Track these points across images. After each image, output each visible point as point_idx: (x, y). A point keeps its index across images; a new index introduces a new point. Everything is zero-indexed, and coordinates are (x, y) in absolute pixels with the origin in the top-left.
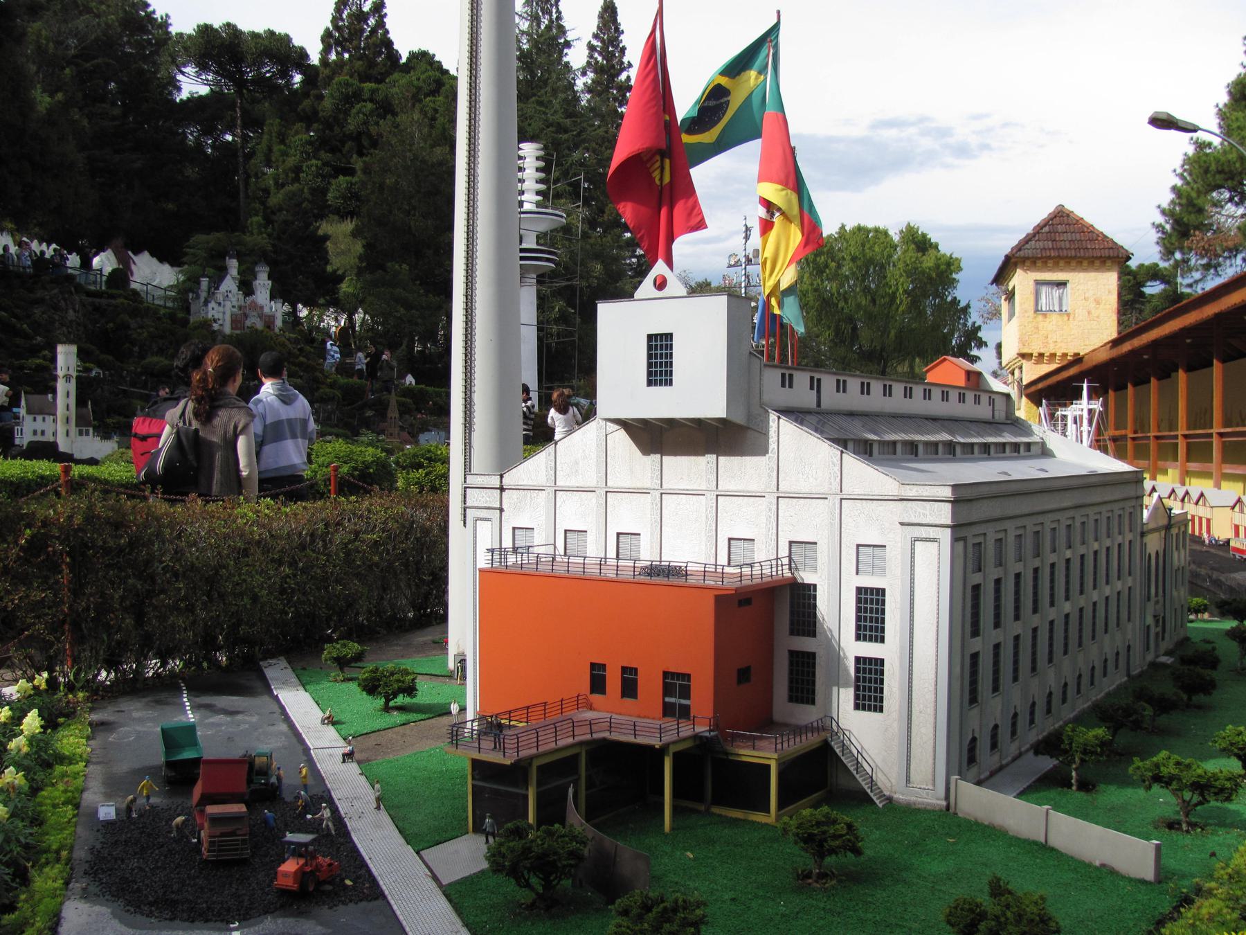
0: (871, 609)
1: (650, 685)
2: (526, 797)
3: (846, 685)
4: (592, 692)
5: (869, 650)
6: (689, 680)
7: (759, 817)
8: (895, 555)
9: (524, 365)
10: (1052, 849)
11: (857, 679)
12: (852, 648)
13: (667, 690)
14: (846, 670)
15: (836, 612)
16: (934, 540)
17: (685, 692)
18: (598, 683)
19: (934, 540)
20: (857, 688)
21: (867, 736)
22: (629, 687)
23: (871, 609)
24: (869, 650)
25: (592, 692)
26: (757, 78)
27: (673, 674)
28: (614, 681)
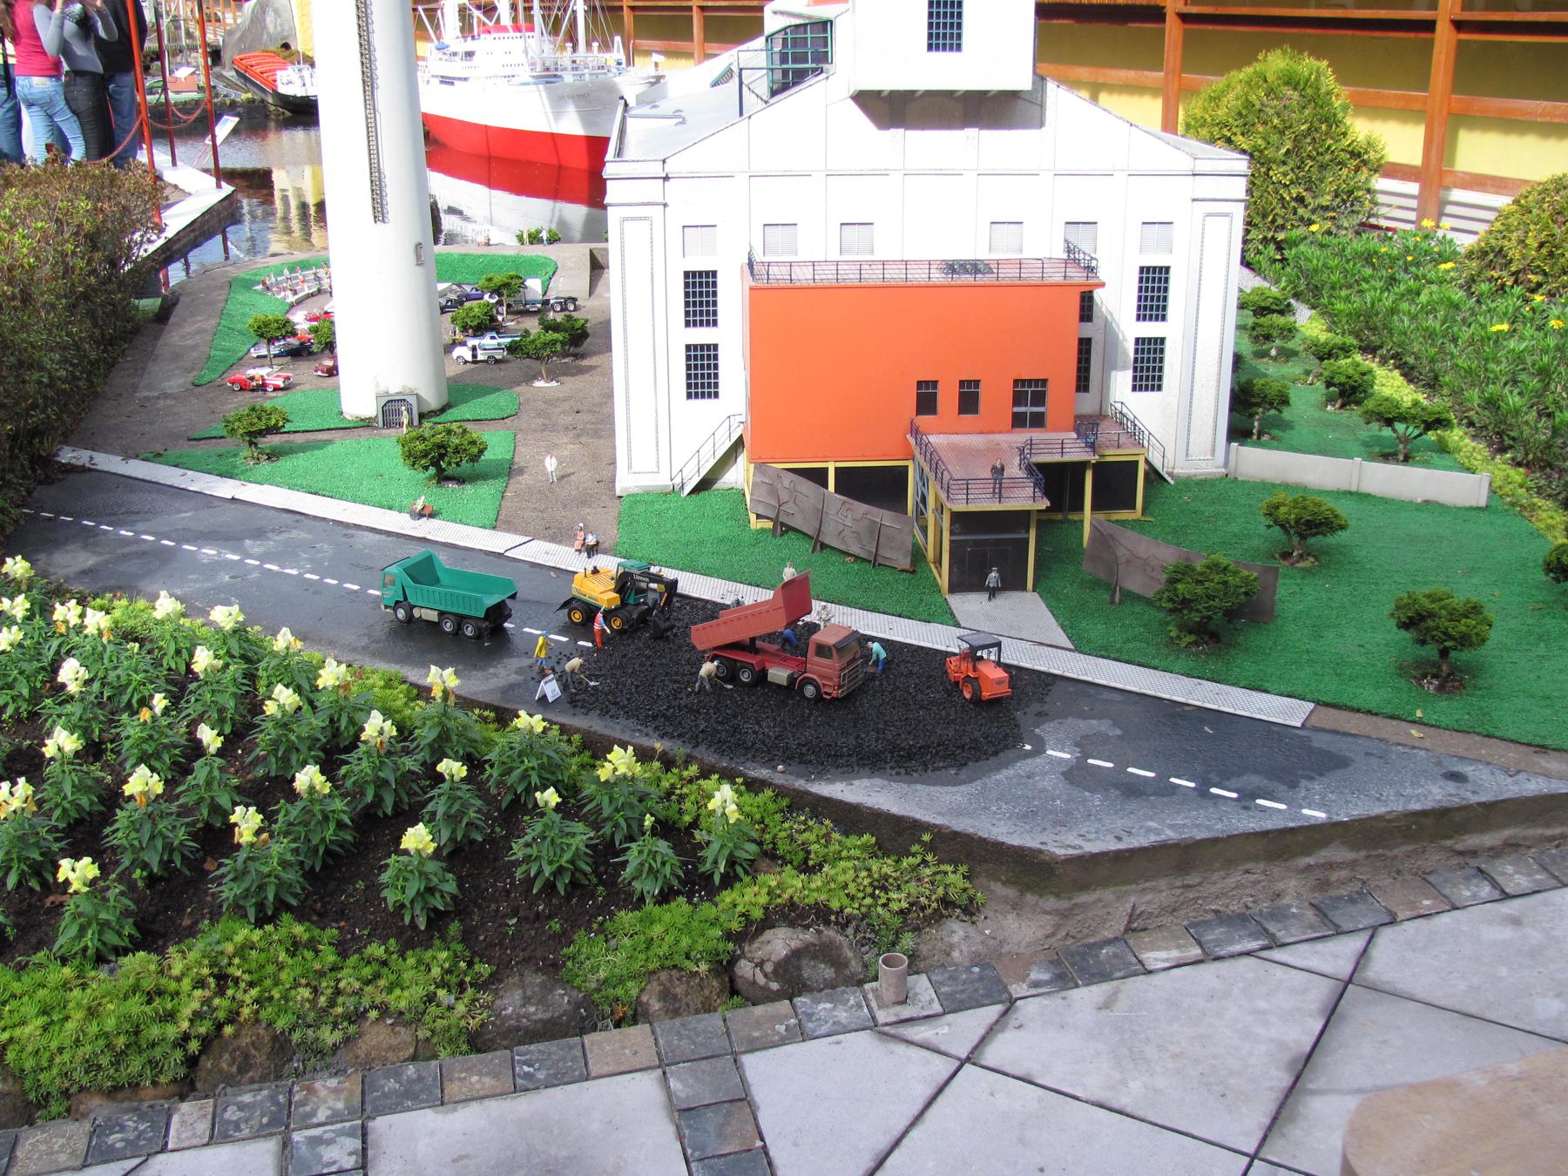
0: (1153, 290)
1: (996, 397)
2: (1026, 541)
3: (1124, 368)
4: (918, 413)
5: (1151, 329)
6: (935, 387)
7: (1124, 515)
8: (1182, 235)
9: (1509, 19)
10: (1369, 495)
11: (1136, 360)
12: (1130, 329)
13: (1018, 399)
14: (1125, 353)
15: (1118, 301)
16: (1226, 215)
17: (1039, 399)
18: (926, 401)
19: (1226, 215)
20: (1135, 369)
21: (1148, 412)
22: (969, 401)
23: (1153, 290)
24: (1151, 329)
25: (918, 413)
26: (177, 8)
27: (1023, 381)
28: (948, 398)
